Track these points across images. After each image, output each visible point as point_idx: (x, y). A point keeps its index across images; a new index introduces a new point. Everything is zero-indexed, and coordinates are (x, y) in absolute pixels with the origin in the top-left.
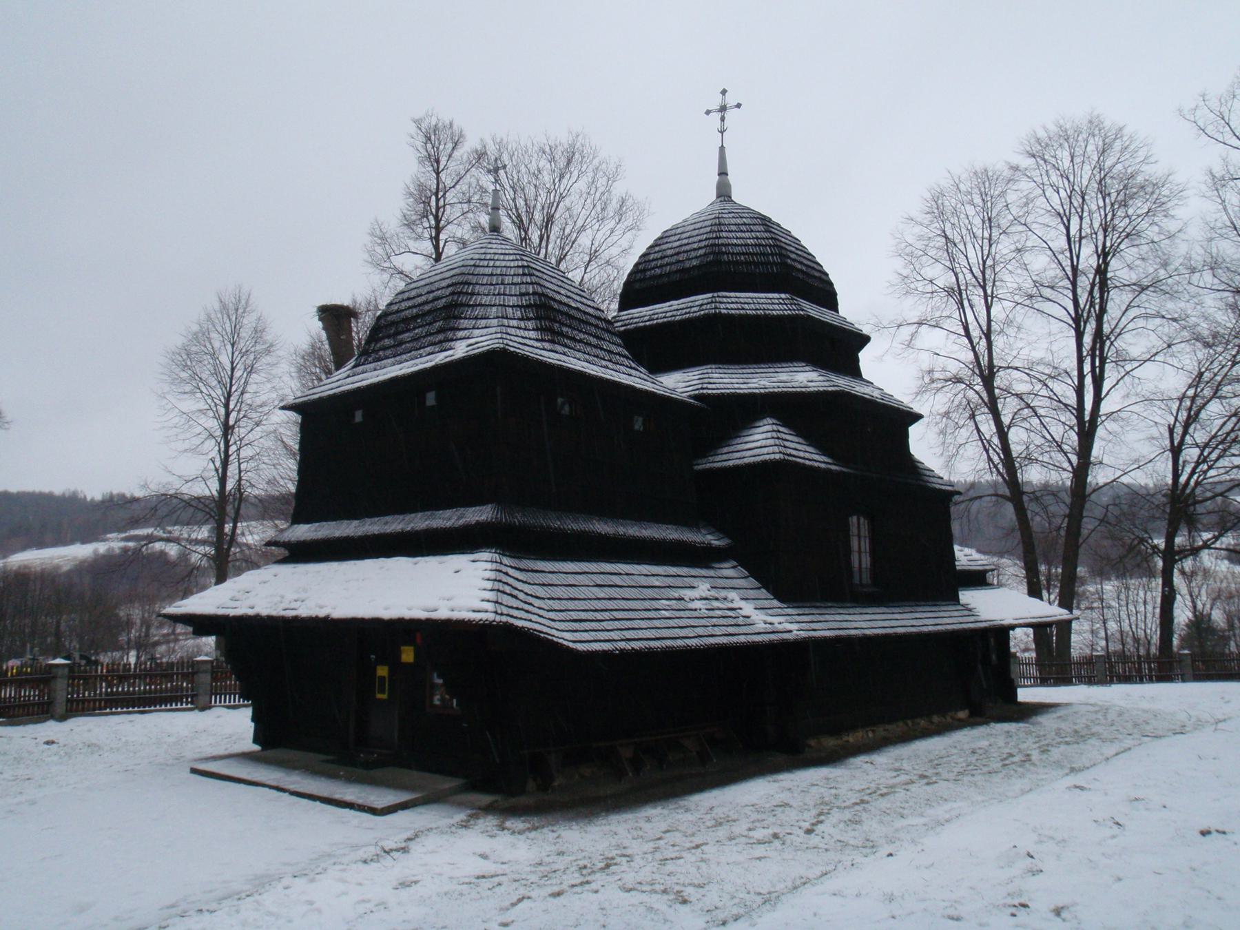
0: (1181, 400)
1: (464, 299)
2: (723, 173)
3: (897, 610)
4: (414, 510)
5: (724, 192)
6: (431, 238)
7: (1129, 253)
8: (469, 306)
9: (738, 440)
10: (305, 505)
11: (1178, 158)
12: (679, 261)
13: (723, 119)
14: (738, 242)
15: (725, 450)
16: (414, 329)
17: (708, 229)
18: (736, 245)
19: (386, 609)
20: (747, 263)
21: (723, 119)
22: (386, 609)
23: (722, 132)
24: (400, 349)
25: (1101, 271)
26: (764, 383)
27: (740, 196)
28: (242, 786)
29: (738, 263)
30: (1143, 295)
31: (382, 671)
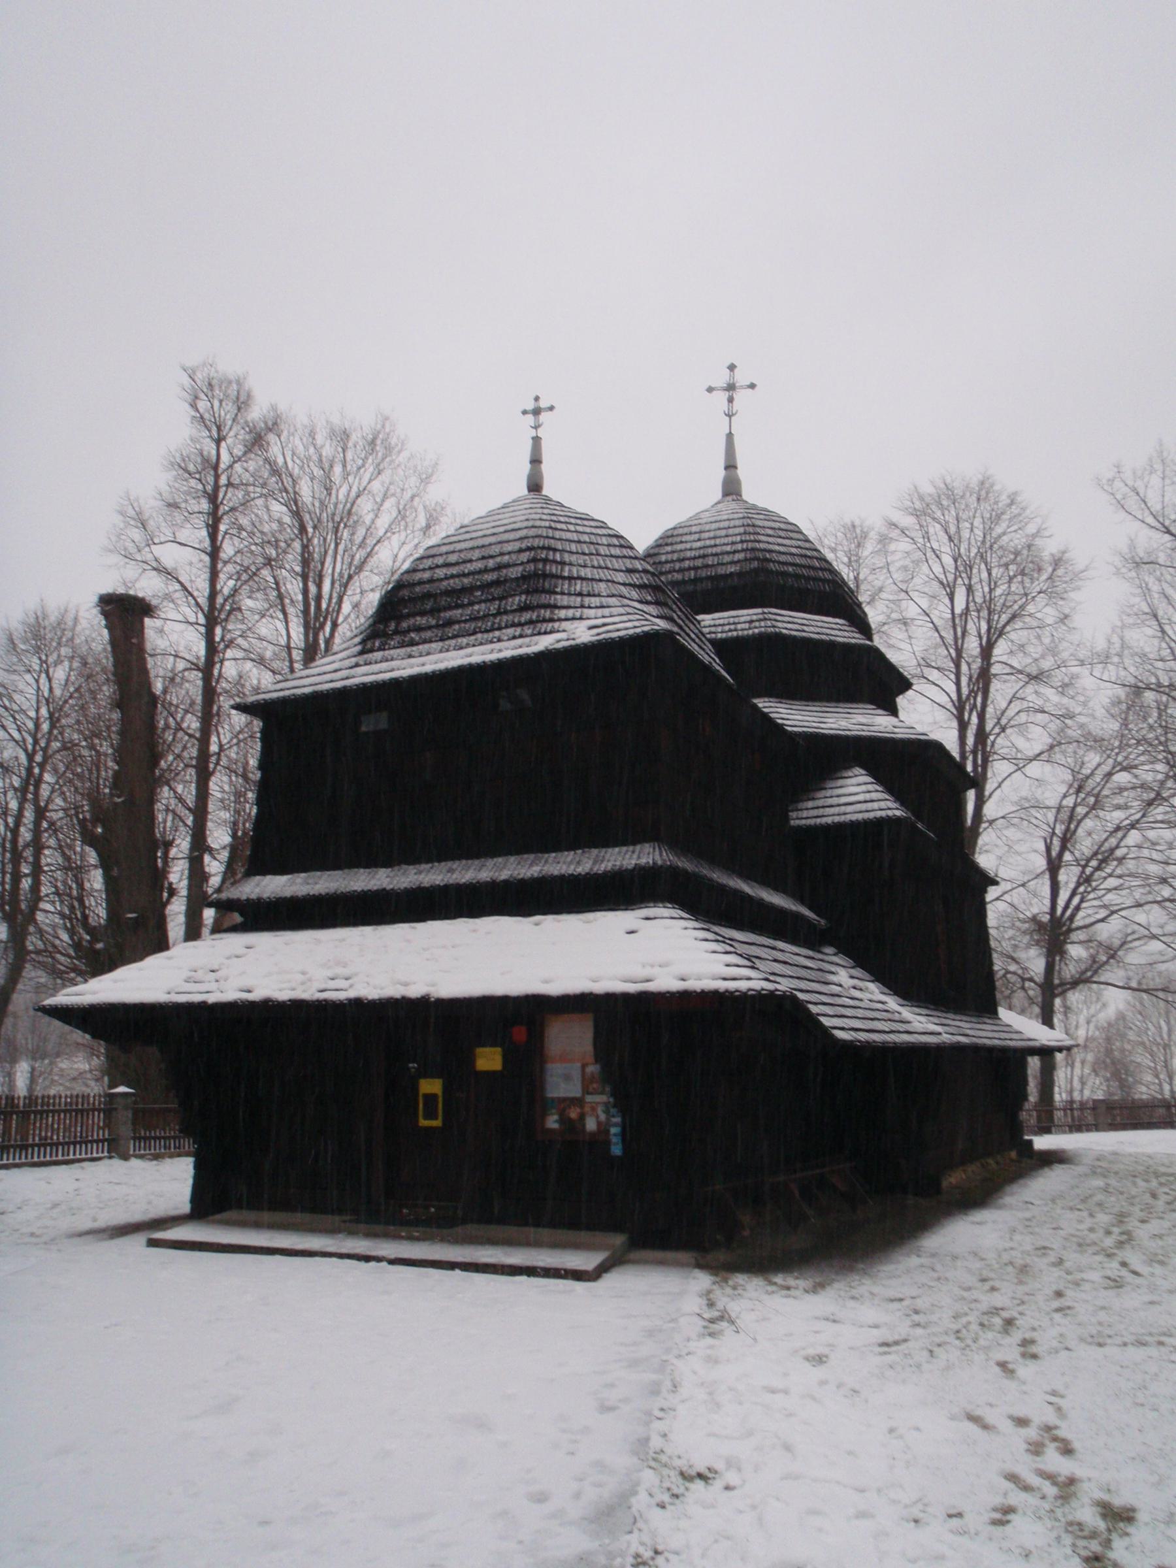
0: (1059, 809)
1: (554, 569)
2: (731, 466)
3: (964, 1018)
4: (493, 853)
5: (731, 488)
6: (208, 525)
7: (1017, 634)
8: (564, 578)
9: (829, 793)
10: (260, 851)
11: (1086, 531)
12: (707, 566)
13: (731, 400)
14: (782, 549)
15: (810, 804)
16: (471, 604)
17: (742, 530)
18: (780, 552)
19: (546, 982)
20: (797, 576)
21: (731, 400)
22: (546, 982)
23: (730, 416)
24: (450, 631)
25: (987, 652)
26: (844, 724)
27: (751, 494)
28: (278, 1257)
29: (784, 574)
30: (1030, 686)
31: (431, 1086)
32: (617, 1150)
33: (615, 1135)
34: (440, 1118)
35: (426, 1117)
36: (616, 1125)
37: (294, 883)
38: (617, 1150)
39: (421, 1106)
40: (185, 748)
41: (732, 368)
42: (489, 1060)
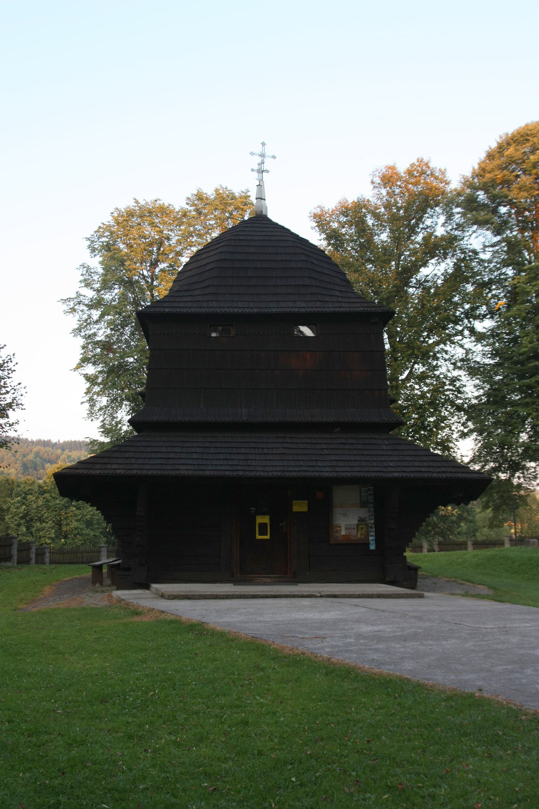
23: (261, 171)
31: (264, 519)
32: (372, 547)
33: (372, 540)
34: (257, 523)
35: (259, 535)
36: (372, 536)
37: (521, 548)
38: (372, 547)
39: (257, 529)
40: (271, 782)
41: (263, 144)
42: (300, 507)
